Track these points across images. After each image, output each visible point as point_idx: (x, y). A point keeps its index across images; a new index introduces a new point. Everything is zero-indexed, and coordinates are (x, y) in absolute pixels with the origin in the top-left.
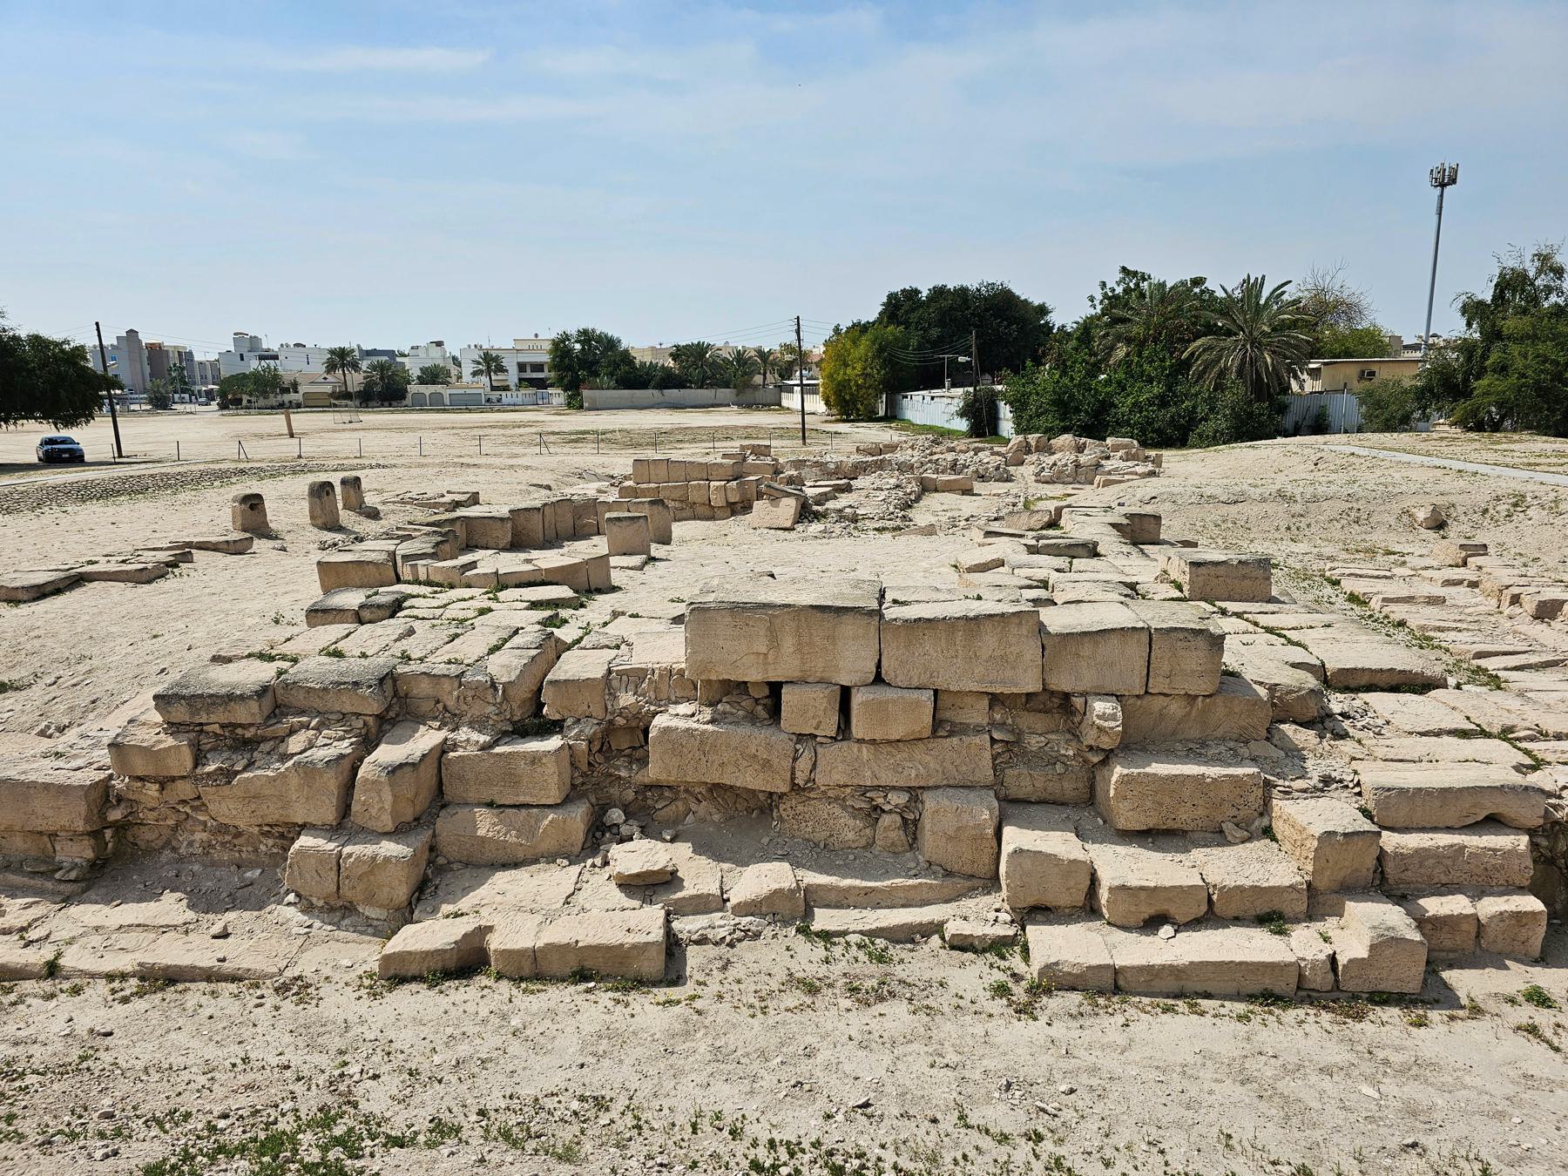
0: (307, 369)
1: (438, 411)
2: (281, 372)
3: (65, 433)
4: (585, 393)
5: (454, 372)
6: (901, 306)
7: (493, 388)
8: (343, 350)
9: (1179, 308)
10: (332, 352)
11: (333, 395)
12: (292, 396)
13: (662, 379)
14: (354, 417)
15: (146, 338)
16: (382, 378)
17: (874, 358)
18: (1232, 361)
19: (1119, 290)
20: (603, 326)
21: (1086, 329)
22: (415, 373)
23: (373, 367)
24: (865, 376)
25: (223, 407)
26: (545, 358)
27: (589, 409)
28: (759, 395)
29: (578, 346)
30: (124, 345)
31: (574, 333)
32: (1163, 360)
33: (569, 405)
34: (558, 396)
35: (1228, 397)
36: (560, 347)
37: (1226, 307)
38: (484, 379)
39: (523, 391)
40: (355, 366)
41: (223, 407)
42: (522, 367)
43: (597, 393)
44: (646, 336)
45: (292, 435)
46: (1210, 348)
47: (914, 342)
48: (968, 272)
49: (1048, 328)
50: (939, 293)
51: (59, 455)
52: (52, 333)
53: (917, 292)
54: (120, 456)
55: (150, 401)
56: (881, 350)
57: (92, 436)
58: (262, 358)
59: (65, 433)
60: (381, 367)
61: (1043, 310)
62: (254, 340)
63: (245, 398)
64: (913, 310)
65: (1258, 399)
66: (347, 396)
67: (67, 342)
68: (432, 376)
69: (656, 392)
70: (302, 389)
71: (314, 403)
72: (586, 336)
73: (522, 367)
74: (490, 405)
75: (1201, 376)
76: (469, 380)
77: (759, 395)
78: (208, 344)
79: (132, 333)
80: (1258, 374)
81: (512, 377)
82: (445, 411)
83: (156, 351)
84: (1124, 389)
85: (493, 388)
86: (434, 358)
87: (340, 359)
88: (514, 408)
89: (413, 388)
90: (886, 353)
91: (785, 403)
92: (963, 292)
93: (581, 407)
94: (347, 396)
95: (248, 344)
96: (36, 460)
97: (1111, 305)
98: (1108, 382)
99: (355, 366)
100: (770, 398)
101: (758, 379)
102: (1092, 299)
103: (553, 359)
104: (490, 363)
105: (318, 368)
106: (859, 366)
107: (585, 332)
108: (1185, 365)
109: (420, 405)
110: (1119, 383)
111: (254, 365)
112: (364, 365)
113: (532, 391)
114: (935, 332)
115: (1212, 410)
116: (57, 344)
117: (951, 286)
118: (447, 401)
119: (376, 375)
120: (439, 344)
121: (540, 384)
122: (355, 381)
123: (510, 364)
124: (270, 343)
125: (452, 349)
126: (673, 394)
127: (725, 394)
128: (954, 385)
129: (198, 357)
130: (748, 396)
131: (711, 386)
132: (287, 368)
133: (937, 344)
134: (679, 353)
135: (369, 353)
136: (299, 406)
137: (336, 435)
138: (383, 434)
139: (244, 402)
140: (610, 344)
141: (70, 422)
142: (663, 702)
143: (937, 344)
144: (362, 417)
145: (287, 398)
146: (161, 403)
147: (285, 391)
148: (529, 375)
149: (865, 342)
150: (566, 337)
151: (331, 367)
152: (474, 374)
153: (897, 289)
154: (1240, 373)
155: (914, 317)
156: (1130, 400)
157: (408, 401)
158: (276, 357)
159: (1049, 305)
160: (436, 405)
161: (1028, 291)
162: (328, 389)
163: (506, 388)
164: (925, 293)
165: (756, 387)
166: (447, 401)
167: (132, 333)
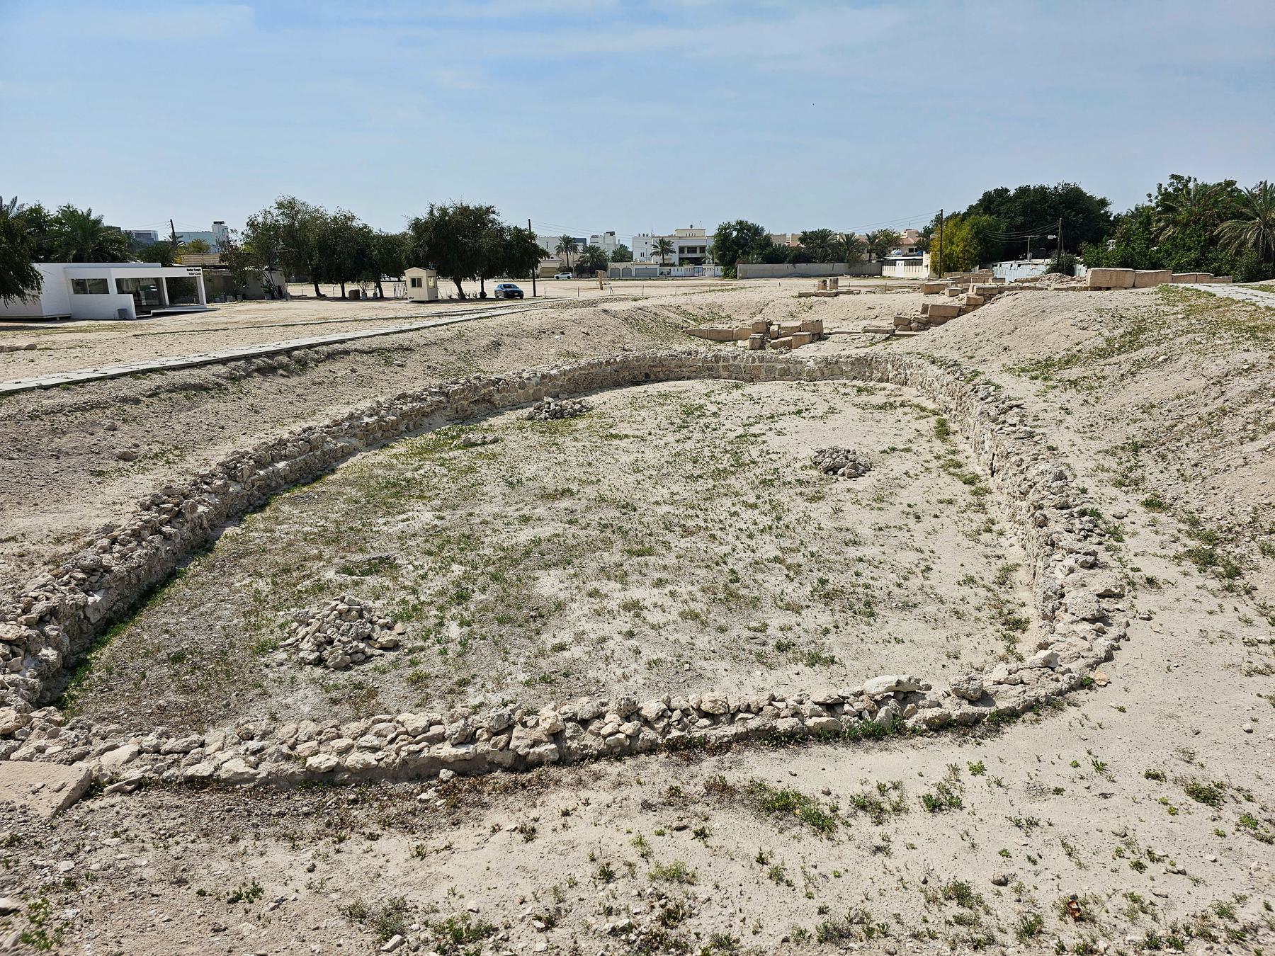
4: (740, 267)
6: (993, 202)
9: (1216, 202)
13: (795, 256)
17: (974, 238)
18: (1251, 237)
19: (1170, 190)
20: (752, 220)
21: (1142, 216)
22: (610, 254)
26: (711, 244)
27: (742, 278)
28: (866, 268)
29: (735, 234)
32: (1200, 236)
35: (1245, 259)
36: (723, 236)
37: (1248, 200)
38: (659, 259)
39: (685, 267)
40: (575, 249)
42: (682, 250)
43: (748, 266)
44: (784, 227)
46: (1235, 228)
47: (1003, 226)
48: (1049, 176)
49: (1107, 215)
50: (1023, 191)
53: (1007, 190)
56: (977, 233)
61: (1103, 203)
64: (1002, 204)
65: (1267, 261)
69: (790, 266)
72: (742, 226)
75: (1226, 246)
77: (866, 268)
80: (1268, 245)
81: (675, 258)
84: (1170, 255)
89: (611, 265)
90: (981, 235)
91: (885, 273)
92: (365, 233)
93: (735, 277)
94: (570, 270)
97: (1163, 199)
98: (1159, 251)
99: (575, 249)
100: (874, 270)
101: (866, 256)
102: (1150, 196)
104: (664, 246)
106: (961, 245)
107: (741, 223)
108: (1213, 241)
109: (616, 275)
110: (1167, 251)
113: (691, 266)
114: (1019, 220)
115: (1232, 268)
117: (375, 231)
118: (634, 274)
120: (612, 234)
121: (698, 262)
122: (573, 258)
123: (675, 247)
126: (802, 267)
127: (839, 266)
128: (1034, 257)
130: (857, 269)
131: (830, 261)
133: (1021, 228)
134: (805, 238)
140: (756, 231)
142: (48, 645)
143: (1021, 228)
149: (966, 225)
150: (728, 226)
153: (991, 189)
154: (1255, 244)
155: (1003, 209)
156: (1174, 262)
159: (1109, 199)
161: (1093, 189)
163: (673, 265)
164: (1012, 192)
165: (863, 262)
166: (634, 274)
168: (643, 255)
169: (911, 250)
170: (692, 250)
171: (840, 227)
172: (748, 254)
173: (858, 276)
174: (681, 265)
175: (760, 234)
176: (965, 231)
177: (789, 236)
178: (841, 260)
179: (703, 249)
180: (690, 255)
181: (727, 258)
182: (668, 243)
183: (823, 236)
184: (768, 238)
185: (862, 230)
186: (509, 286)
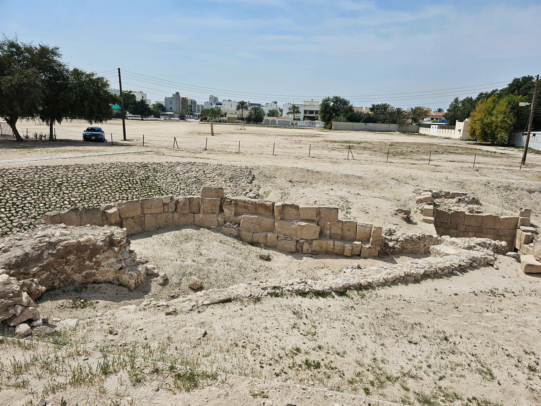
0: (230, 109)
1: (274, 127)
2: (222, 109)
3: (95, 125)
4: (334, 123)
5: (280, 113)
7: (294, 119)
8: (243, 102)
10: (240, 103)
11: (238, 119)
12: (224, 118)
13: (367, 118)
14: (242, 127)
15: (182, 96)
16: (255, 113)
22: (267, 112)
23: (253, 109)
24: (503, 121)
25: (201, 120)
26: (318, 109)
27: (334, 130)
28: (409, 128)
29: (332, 103)
30: (175, 97)
31: (332, 98)
33: (325, 128)
34: (319, 123)
36: (325, 105)
38: (291, 116)
39: (306, 121)
40: (246, 108)
41: (201, 120)
42: (305, 112)
44: (362, 104)
45: (213, 134)
51: (94, 138)
52: (87, 69)
54: (125, 139)
55: (179, 117)
57: (110, 129)
58: (217, 104)
59: (95, 125)
60: (255, 109)
62: (216, 99)
63: (208, 117)
66: (242, 119)
67: (93, 75)
68: (273, 113)
70: (227, 116)
71: (231, 121)
72: (337, 100)
73: (305, 112)
74: (293, 126)
76: (287, 117)
77: (409, 128)
78: (201, 100)
79: (178, 93)
82: (276, 127)
83: (184, 100)
85: (294, 119)
86: (273, 107)
87: (242, 105)
88: (302, 128)
89: (266, 118)
92: (510, 85)
93: (331, 128)
94: (242, 119)
95: (214, 99)
96: (81, 138)
99: (246, 108)
103: (322, 108)
104: (295, 109)
105: (234, 108)
106: (501, 117)
107: (336, 98)
109: (268, 124)
111: (214, 106)
112: (249, 108)
113: (309, 121)
116: (88, 76)
119: (253, 112)
120: (276, 103)
121: (313, 119)
122: (246, 114)
123: (302, 110)
124: (220, 100)
125: (280, 105)
126: (371, 125)
129: (198, 103)
130: (404, 128)
131: (388, 122)
132: (224, 109)
135: (252, 104)
136: (226, 122)
137: (232, 135)
138: (253, 136)
139: (208, 119)
140: (345, 103)
141: (100, 120)
144: (246, 127)
145: (222, 118)
146: (182, 118)
147: (222, 116)
148: (308, 115)
150: (328, 100)
151: (238, 108)
152: (288, 114)
153: (520, 76)
157: (263, 122)
158: (221, 104)
160: (273, 124)
162: (236, 116)
163: (299, 120)
167: (178, 93)
168: (230, 109)
169: (432, 119)
170: (311, 112)
171: (394, 104)
172: (339, 115)
174: (304, 119)
175: (347, 104)
176: (503, 105)
177: (364, 108)
178: (394, 122)
179: (317, 112)
180: (310, 115)
181: (326, 118)
182: (297, 108)
183: (385, 107)
184: (351, 107)
185: (406, 107)
186: (93, 129)
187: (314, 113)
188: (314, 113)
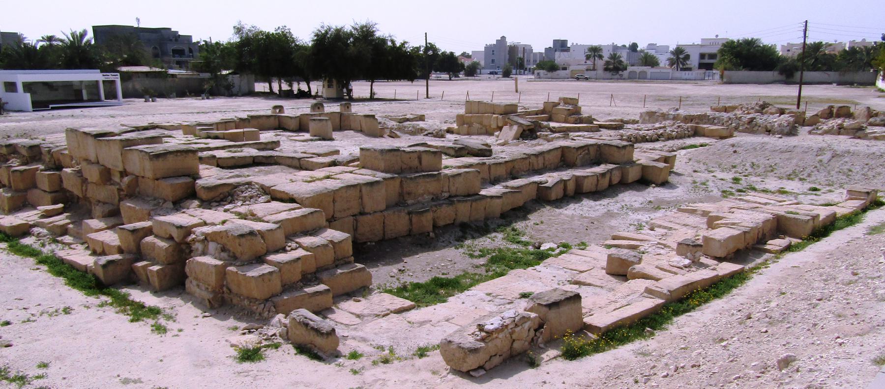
15: (510, 41)
42: (702, 56)
54: (427, 97)
73: (702, 56)
78: (540, 45)
83: (513, 49)
87: (595, 52)
113: (703, 71)
148: (707, 61)
167: (503, 38)
173: (851, 84)
187: (707, 57)
188: (707, 57)
